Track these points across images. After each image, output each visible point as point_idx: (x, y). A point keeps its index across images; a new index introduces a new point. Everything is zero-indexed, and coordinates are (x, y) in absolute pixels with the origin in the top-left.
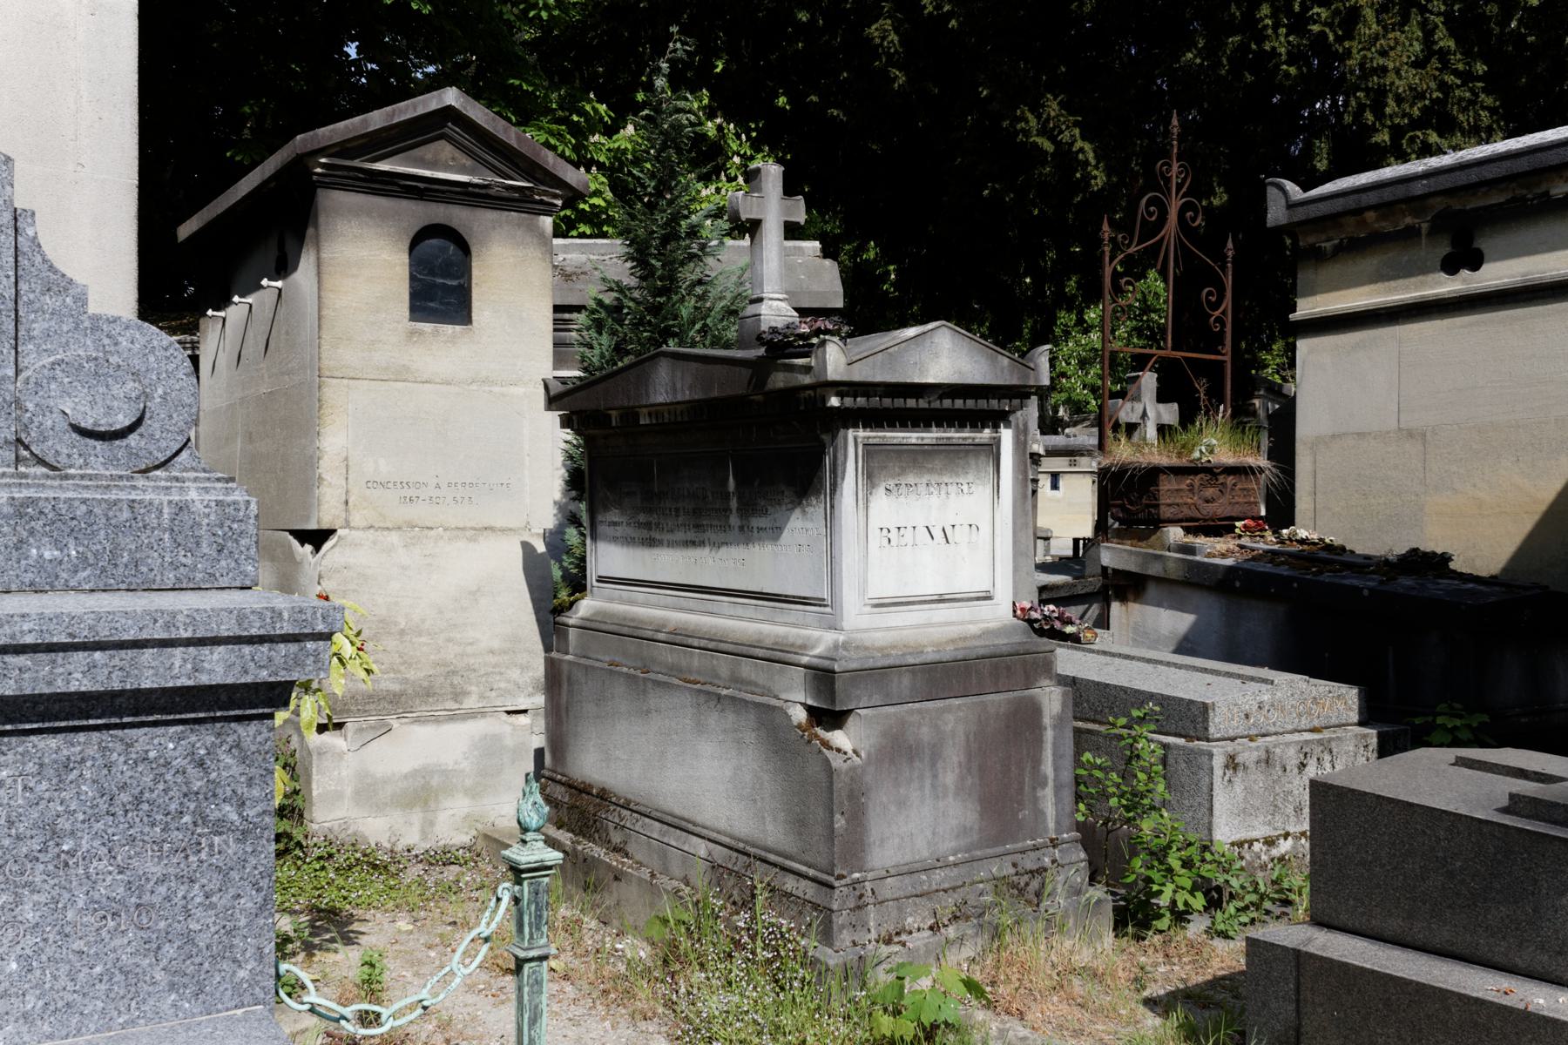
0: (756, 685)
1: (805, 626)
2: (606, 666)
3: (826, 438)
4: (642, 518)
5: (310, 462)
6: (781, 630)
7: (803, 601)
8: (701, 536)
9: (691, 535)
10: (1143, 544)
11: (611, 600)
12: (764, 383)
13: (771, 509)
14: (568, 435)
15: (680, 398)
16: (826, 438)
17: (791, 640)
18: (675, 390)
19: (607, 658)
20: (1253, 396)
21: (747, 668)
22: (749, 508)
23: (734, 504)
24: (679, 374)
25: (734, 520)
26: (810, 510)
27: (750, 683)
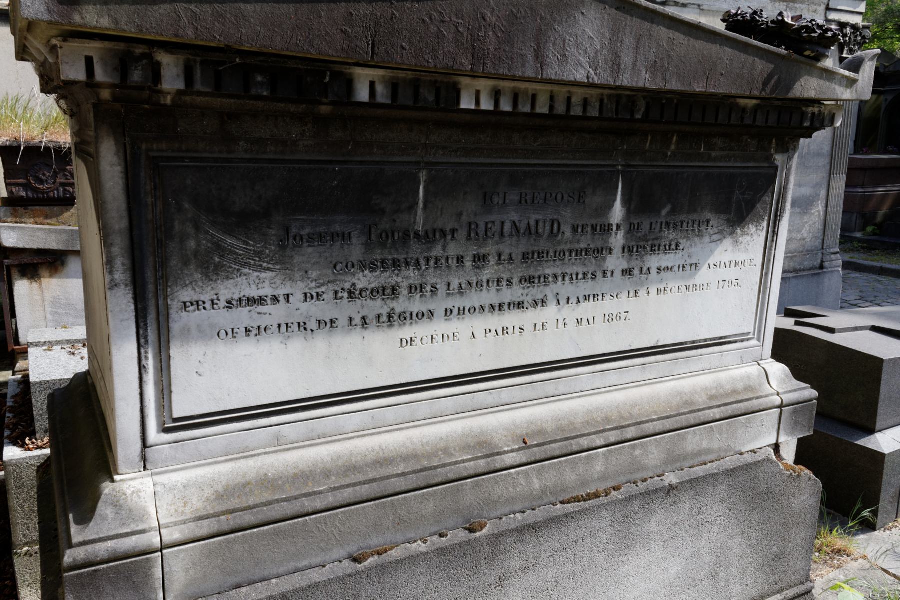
0: (708, 451)
1: (724, 368)
2: (348, 566)
3: (779, 159)
4: (364, 280)
5: (42, 590)
6: (706, 381)
7: (720, 342)
8: (536, 292)
9: (516, 293)
10: (54, 221)
11: (245, 453)
12: (789, 88)
13: (684, 243)
14: (53, 97)
15: (626, 80)
16: (779, 159)
17: (728, 388)
18: (616, 67)
19: (339, 552)
20: (166, 105)
21: (694, 440)
22: (642, 244)
23: (618, 240)
24: (629, 40)
25: (615, 262)
26: (745, 240)
27: (699, 454)
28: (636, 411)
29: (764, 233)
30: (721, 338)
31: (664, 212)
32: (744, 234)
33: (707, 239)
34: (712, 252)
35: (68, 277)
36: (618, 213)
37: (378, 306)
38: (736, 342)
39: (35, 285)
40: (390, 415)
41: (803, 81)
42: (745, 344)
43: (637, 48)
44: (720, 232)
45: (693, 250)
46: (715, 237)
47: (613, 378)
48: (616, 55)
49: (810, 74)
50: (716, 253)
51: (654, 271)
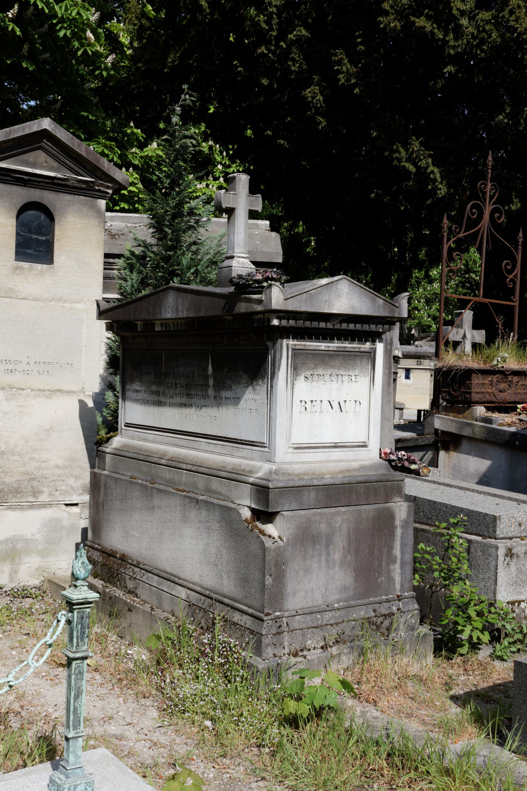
0: (221, 494)
1: (252, 459)
3: (269, 344)
12: (233, 309)
13: (234, 387)
15: (180, 315)
16: (269, 344)
21: (215, 484)
23: (211, 382)
24: (180, 301)
25: (211, 392)
26: (258, 388)
27: (217, 493)
28: (206, 463)
29: (266, 385)
30: (252, 442)
31: (225, 370)
32: (257, 385)
33: (242, 386)
34: (244, 393)
35: (461, 453)
36: (210, 370)
37: (156, 398)
38: (259, 446)
39: (447, 455)
40: (159, 438)
41: (238, 305)
42: (263, 449)
43: (183, 304)
44: (247, 383)
45: (237, 390)
46: (245, 385)
47: (212, 448)
48: (177, 307)
49: (241, 301)
50: (246, 393)
51: (224, 399)
